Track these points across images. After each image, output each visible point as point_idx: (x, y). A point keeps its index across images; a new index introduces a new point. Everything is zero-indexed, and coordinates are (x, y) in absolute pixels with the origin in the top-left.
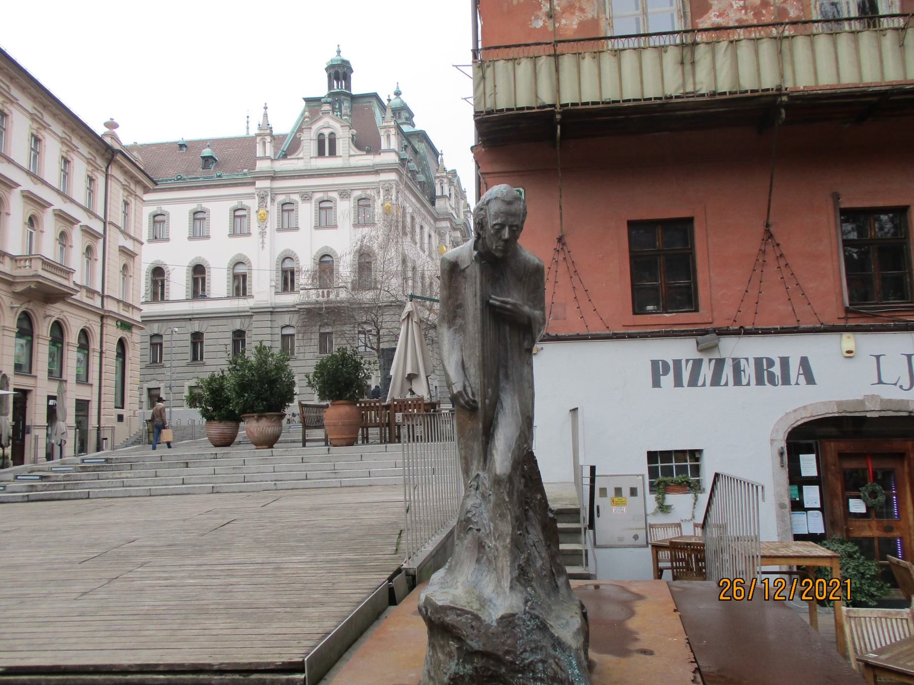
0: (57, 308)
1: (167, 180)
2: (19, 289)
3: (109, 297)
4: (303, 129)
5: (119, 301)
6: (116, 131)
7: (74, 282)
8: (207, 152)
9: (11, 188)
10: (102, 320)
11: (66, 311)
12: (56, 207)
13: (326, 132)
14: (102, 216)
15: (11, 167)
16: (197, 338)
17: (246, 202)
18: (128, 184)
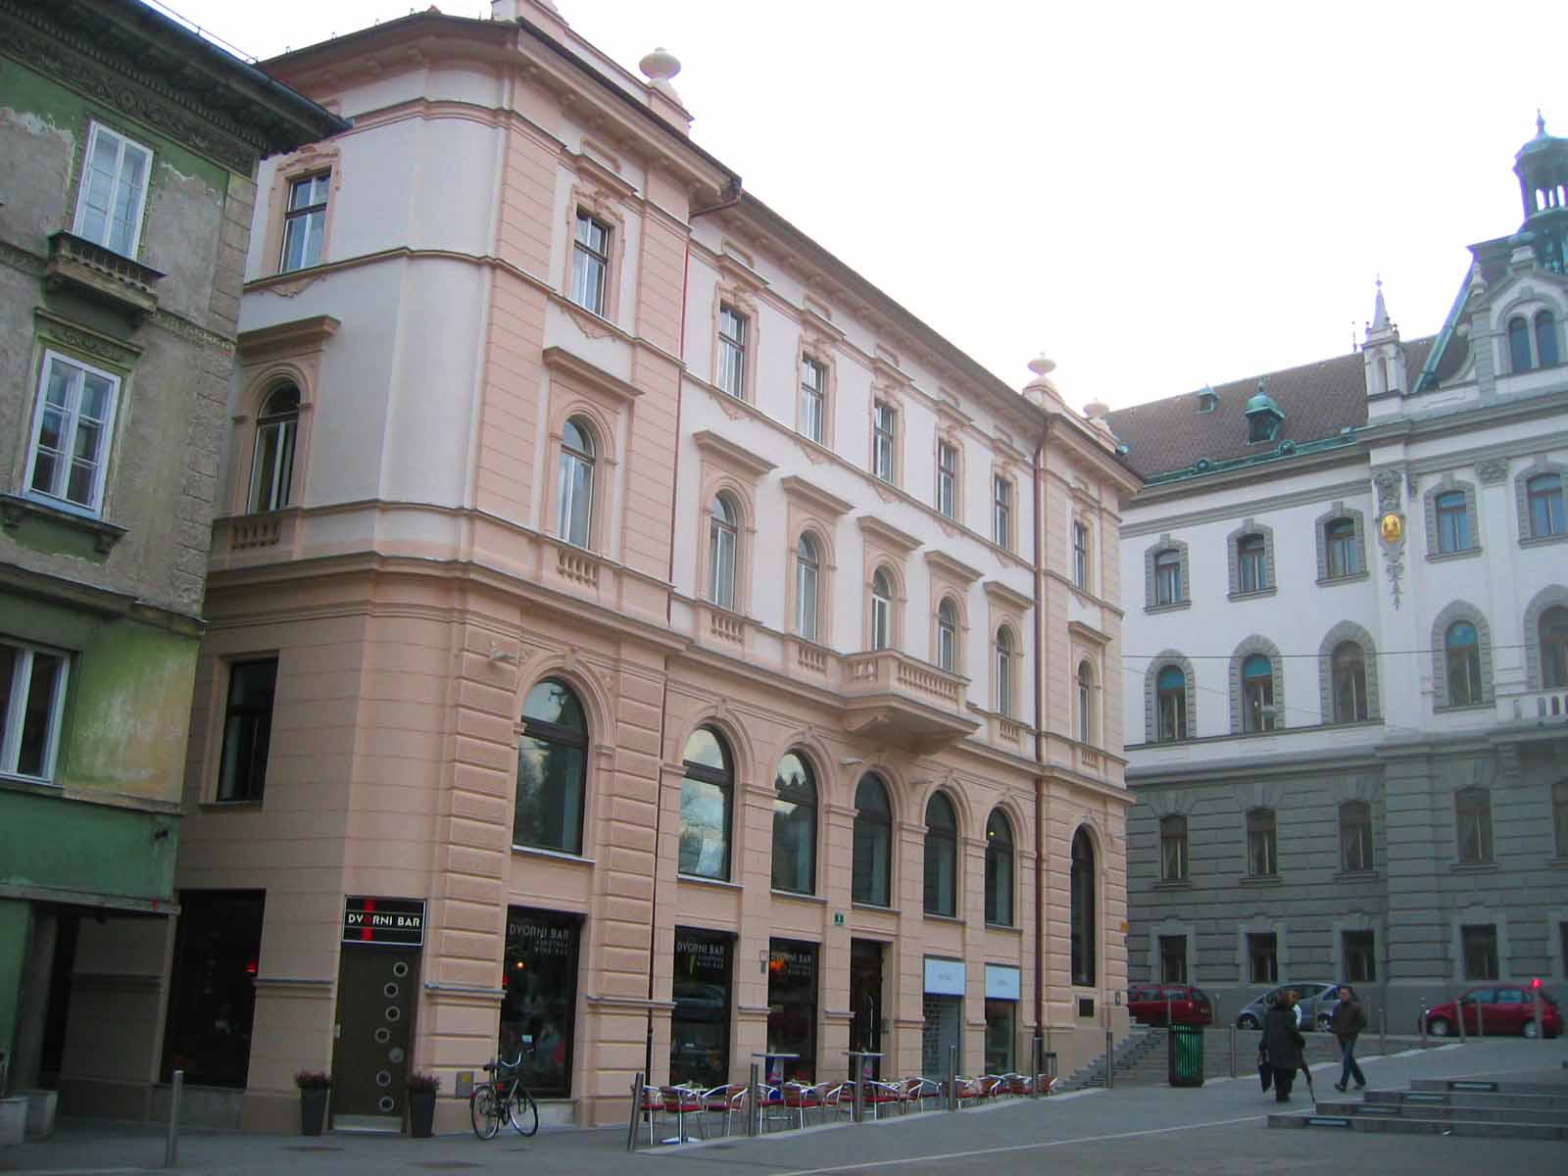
0: (939, 764)
1: (1177, 476)
2: (858, 723)
3: (1049, 735)
4: (1470, 315)
5: (1072, 745)
6: (1049, 376)
7: (968, 703)
8: (1257, 403)
9: (758, 473)
10: (1038, 789)
11: (733, 700)
12: (785, 471)
13: (1528, 311)
14: (1030, 560)
15: (758, 428)
16: (1261, 823)
17: (1351, 503)
18: (1083, 487)
